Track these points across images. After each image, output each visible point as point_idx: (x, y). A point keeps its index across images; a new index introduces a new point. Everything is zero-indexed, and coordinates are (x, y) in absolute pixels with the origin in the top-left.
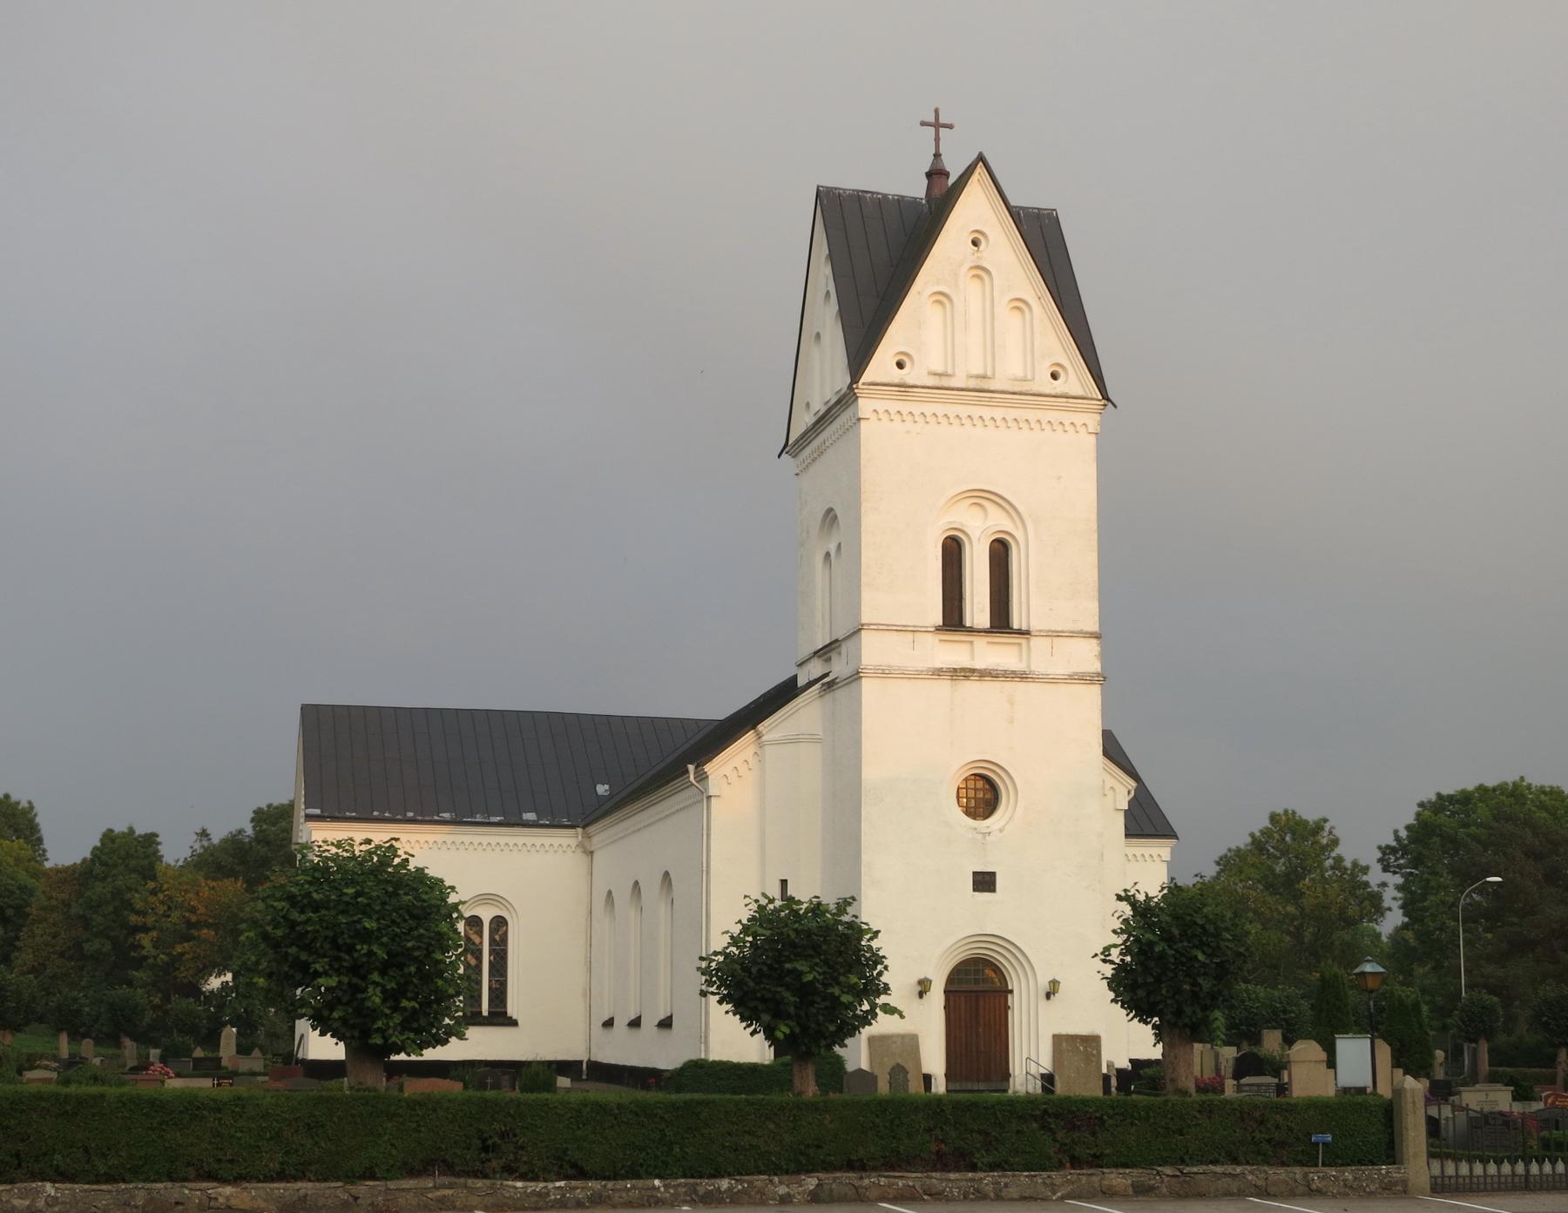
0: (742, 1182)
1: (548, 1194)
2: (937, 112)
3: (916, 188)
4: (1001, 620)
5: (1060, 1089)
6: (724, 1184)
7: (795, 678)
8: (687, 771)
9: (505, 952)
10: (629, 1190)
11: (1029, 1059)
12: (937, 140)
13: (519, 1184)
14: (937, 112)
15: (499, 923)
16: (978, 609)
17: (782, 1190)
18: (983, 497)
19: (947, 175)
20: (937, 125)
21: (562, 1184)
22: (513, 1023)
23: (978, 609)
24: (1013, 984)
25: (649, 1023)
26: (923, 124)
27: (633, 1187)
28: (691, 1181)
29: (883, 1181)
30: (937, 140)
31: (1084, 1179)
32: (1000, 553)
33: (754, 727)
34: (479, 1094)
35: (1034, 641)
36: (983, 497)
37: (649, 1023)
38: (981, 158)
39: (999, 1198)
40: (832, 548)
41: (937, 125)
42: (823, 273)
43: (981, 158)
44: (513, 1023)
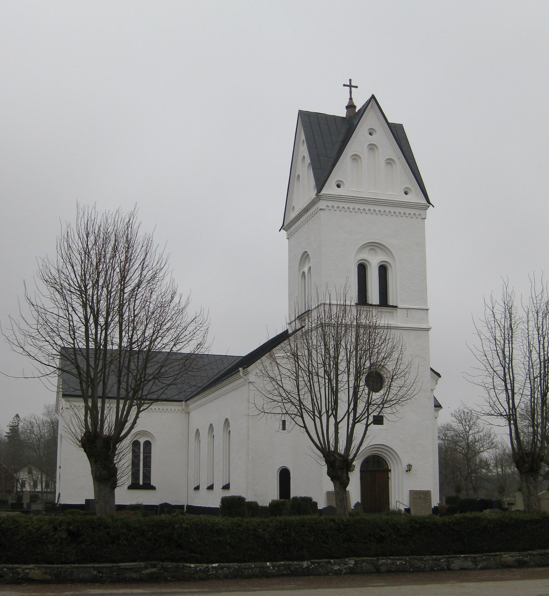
0: (313, 563)
1: (208, 571)
2: (350, 80)
3: (343, 113)
4: (384, 301)
5: (413, 512)
6: (305, 564)
7: (287, 331)
8: (239, 371)
9: (150, 457)
10: (253, 568)
11: (399, 499)
12: (351, 92)
13: (193, 565)
14: (350, 80)
15: (148, 444)
16: (374, 296)
17: (336, 568)
18: (374, 246)
19: (355, 107)
20: (350, 86)
21: (216, 565)
22: (154, 488)
23: (374, 296)
24: (391, 466)
25: (203, 487)
26: (344, 85)
27: (256, 567)
28: (287, 563)
29: (389, 561)
30: (351, 92)
31: (492, 558)
32: (383, 270)
33: (270, 351)
34: (298, 518)
35: (399, 310)
36: (374, 246)
37: (203, 487)
38: (373, 97)
39: (449, 569)
40: (306, 270)
41: (350, 86)
42: (304, 150)
43: (373, 97)
44: (154, 488)
